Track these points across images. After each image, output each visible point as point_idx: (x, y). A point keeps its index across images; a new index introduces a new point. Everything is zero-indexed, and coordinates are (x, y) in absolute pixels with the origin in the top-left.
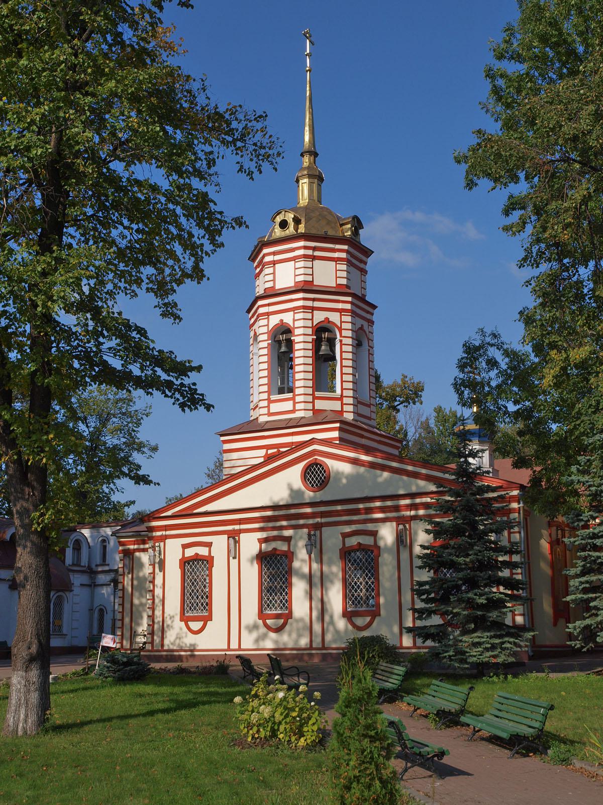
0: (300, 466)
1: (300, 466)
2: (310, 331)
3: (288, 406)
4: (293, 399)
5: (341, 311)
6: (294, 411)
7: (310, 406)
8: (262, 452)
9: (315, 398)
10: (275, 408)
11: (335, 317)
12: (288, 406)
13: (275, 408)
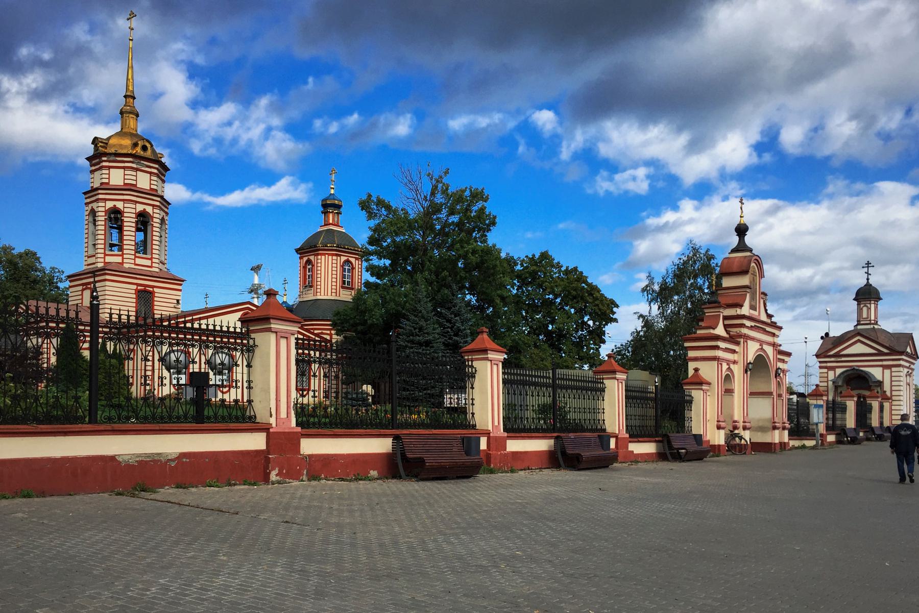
0: (241, 313)
1: (241, 313)
2: (134, 216)
3: (148, 263)
4: (122, 255)
5: (153, 206)
6: (151, 267)
7: (102, 260)
8: (135, 287)
9: (136, 257)
10: (138, 261)
11: (149, 209)
12: (148, 263)
13: (138, 261)
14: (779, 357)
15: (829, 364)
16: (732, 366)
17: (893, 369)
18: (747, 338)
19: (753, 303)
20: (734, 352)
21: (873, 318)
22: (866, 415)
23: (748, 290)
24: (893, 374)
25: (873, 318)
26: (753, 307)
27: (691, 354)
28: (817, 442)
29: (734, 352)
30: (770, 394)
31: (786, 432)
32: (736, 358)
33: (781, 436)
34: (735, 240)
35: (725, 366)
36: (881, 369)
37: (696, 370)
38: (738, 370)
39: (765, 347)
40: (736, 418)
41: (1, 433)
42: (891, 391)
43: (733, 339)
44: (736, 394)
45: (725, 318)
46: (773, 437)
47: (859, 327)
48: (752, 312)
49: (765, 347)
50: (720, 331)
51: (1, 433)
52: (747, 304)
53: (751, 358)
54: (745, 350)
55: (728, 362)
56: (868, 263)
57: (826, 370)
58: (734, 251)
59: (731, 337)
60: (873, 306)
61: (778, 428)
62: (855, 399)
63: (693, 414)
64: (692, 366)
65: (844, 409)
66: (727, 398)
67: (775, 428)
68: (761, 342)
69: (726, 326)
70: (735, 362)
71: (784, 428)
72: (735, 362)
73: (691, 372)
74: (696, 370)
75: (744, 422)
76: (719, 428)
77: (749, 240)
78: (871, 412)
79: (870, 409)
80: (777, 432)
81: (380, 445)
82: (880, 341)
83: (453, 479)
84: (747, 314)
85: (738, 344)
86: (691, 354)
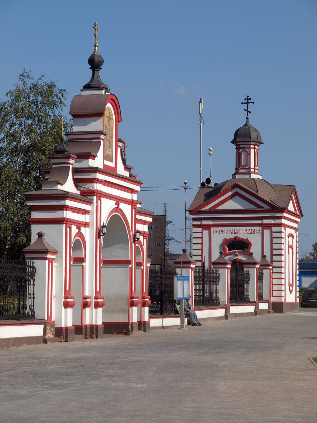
14: (139, 217)
15: (204, 222)
16: (83, 230)
17: (274, 229)
18: (101, 195)
19: (108, 152)
20: (86, 212)
21: (240, 171)
22: (243, 286)
23: (102, 137)
24: (274, 235)
25: (240, 171)
26: (107, 157)
27: (35, 215)
28: (182, 322)
29: (86, 212)
30: (129, 262)
31: (146, 309)
32: (88, 221)
33: (141, 314)
34: (86, 75)
35: (74, 228)
36: (260, 228)
37: (40, 235)
38: (89, 234)
39: (123, 206)
40: (87, 294)
41: (1, 324)
42: (272, 255)
43: (87, 196)
44: (87, 264)
45: (76, 171)
46: (129, 314)
47: (237, 177)
48: (107, 163)
49: (123, 206)
50: (69, 186)
51: (1, 324)
52: (100, 154)
53: (104, 220)
54: (99, 210)
55: (79, 225)
56: (248, 99)
57: (200, 229)
58: (87, 87)
59: (83, 194)
60: (252, 151)
61: (136, 305)
62: (229, 266)
63: (37, 289)
64: (35, 229)
65: (216, 279)
66: (76, 269)
67: (132, 304)
68: (118, 200)
69: (77, 182)
70: (86, 225)
71: (144, 304)
72: (86, 225)
73: (34, 237)
74: (40, 235)
75: (96, 298)
76: (67, 305)
77: (104, 75)
78: (248, 282)
79: (247, 279)
80: (135, 309)
81: (134, 300)
82: (260, 194)
83: (109, 161)
84: (101, 166)
85: (90, 203)
86: (35, 215)
